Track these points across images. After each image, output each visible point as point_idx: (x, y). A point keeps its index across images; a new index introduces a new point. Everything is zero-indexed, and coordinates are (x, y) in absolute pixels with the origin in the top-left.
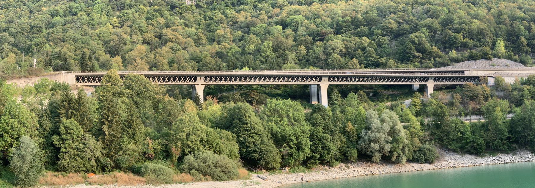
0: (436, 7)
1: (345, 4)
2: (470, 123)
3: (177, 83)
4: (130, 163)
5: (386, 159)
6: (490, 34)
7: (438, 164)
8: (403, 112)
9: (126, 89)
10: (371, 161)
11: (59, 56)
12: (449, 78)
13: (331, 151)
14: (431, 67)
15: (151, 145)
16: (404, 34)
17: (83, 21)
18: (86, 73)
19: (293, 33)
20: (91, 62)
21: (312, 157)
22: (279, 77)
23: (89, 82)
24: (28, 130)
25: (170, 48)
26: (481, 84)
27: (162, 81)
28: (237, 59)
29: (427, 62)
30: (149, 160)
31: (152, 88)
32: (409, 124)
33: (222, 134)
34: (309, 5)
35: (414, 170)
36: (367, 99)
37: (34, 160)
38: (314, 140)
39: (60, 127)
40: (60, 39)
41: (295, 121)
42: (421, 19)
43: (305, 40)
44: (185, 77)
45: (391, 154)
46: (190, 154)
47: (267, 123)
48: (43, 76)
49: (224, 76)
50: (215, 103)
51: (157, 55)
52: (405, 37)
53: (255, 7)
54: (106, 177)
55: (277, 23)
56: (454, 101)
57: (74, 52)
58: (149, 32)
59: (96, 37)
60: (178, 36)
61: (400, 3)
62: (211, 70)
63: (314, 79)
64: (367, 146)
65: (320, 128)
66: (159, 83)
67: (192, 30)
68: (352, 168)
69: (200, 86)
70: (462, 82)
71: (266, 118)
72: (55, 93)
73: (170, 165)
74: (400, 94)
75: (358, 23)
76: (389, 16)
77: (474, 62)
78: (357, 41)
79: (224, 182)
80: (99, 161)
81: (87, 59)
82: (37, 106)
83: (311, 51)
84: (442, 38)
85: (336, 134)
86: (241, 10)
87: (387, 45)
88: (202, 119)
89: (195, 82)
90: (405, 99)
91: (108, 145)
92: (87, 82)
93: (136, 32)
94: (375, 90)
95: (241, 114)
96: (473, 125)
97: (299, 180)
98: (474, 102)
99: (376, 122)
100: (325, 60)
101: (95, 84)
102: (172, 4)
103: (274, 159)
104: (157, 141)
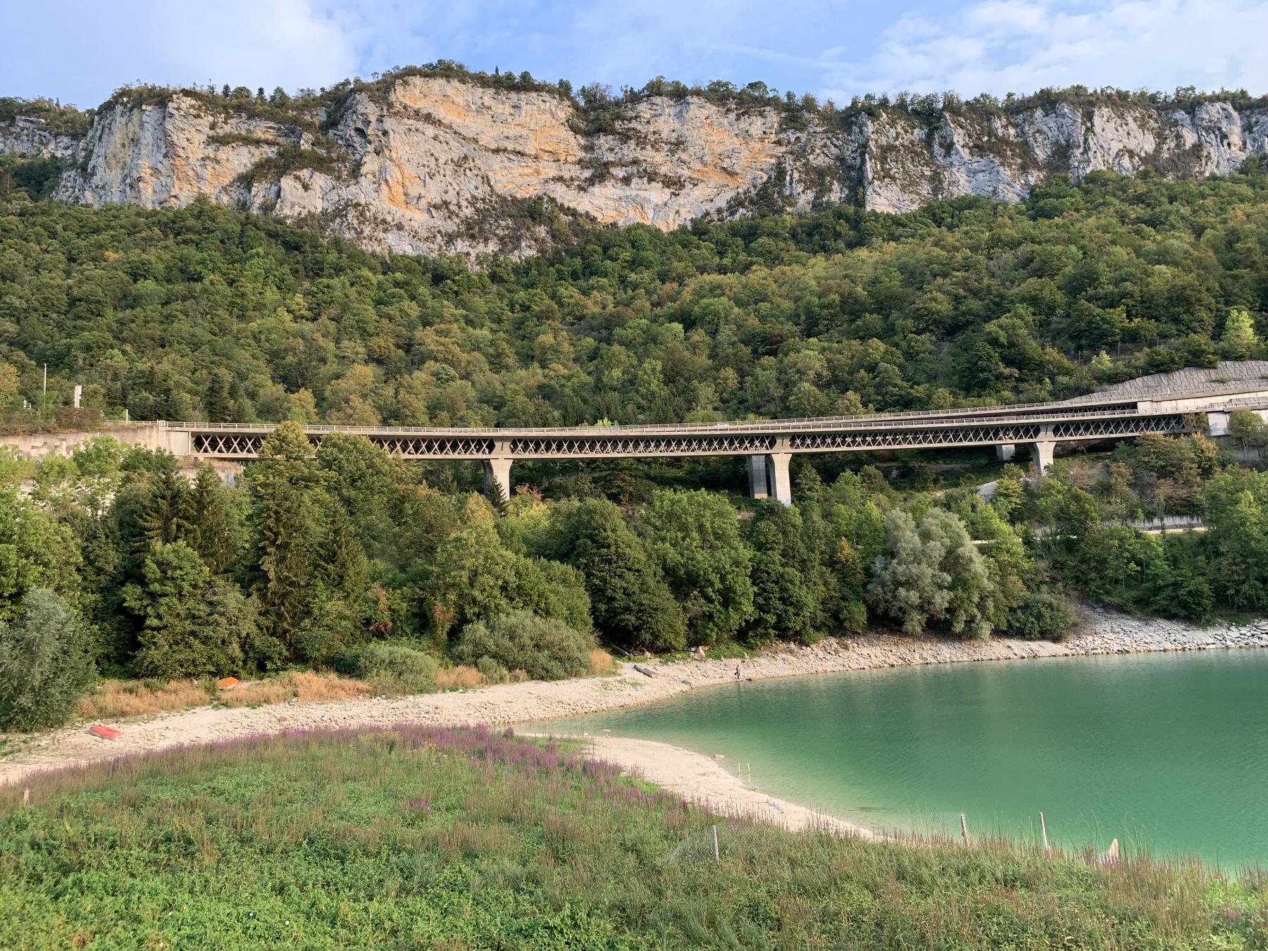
0: (1049, 247)
1: (824, 264)
2: (1164, 538)
3: (447, 457)
4: (329, 647)
5: (939, 628)
6: (1208, 299)
7: (1077, 642)
8: (976, 513)
9: (324, 468)
10: (900, 631)
11: (149, 381)
12: (1097, 425)
13: (802, 608)
14: (1043, 401)
15: (383, 600)
16: (969, 323)
17: (218, 298)
18: (222, 428)
19: (708, 339)
20: (236, 401)
21: (758, 622)
22: (679, 440)
23: (228, 451)
24: (48, 573)
25: (432, 375)
26: (1188, 434)
27: (413, 451)
28: (585, 401)
29: (1030, 388)
30: (378, 637)
31: (387, 467)
32: (993, 541)
33: (551, 571)
34: (742, 272)
35: (1012, 656)
36: (886, 484)
37: (65, 652)
38: (763, 582)
39: (144, 562)
40: (153, 339)
41: (716, 539)
42: (1012, 282)
43: (735, 355)
44: (467, 442)
45: (952, 615)
46: (478, 619)
47: (654, 544)
48: (100, 430)
49: (554, 439)
50: (536, 502)
51: (402, 391)
52: (973, 332)
53: (623, 280)
54: (269, 686)
55: (672, 318)
56: (1113, 481)
57: (189, 374)
58: (381, 334)
59: (249, 341)
60: (450, 346)
61: (956, 249)
62: (526, 426)
63: (757, 443)
64: (889, 596)
65: (775, 553)
66: (406, 456)
67: (483, 333)
68: (856, 649)
69: (501, 462)
70: (1132, 431)
71: (652, 533)
72: (135, 476)
73: (429, 648)
74: (967, 470)
75: (857, 307)
76: (930, 284)
77: (1163, 377)
78: (856, 351)
79: (558, 682)
80: (252, 646)
81: (225, 393)
82: (79, 508)
83: (748, 378)
84: (1069, 325)
85: (813, 567)
86: (593, 288)
87: (930, 353)
88: (506, 537)
89: (490, 453)
90: (980, 480)
91: (274, 604)
92: (224, 449)
93: (351, 333)
94: (902, 462)
95: (594, 524)
96: (1172, 542)
97: (729, 677)
98: (1170, 481)
99: (909, 538)
100: (781, 398)
101: (244, 455)
102: (436, 270)
103: (670, 626)
104: (399, 591)
